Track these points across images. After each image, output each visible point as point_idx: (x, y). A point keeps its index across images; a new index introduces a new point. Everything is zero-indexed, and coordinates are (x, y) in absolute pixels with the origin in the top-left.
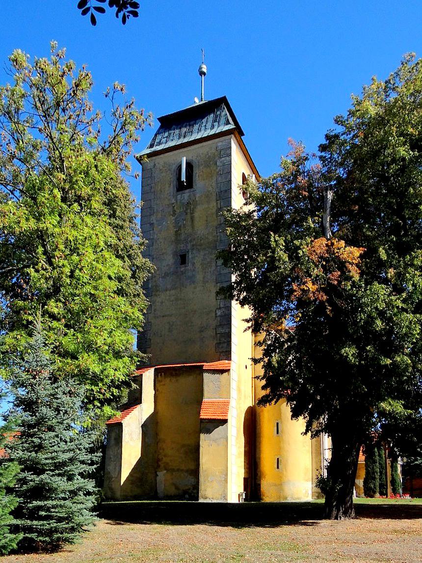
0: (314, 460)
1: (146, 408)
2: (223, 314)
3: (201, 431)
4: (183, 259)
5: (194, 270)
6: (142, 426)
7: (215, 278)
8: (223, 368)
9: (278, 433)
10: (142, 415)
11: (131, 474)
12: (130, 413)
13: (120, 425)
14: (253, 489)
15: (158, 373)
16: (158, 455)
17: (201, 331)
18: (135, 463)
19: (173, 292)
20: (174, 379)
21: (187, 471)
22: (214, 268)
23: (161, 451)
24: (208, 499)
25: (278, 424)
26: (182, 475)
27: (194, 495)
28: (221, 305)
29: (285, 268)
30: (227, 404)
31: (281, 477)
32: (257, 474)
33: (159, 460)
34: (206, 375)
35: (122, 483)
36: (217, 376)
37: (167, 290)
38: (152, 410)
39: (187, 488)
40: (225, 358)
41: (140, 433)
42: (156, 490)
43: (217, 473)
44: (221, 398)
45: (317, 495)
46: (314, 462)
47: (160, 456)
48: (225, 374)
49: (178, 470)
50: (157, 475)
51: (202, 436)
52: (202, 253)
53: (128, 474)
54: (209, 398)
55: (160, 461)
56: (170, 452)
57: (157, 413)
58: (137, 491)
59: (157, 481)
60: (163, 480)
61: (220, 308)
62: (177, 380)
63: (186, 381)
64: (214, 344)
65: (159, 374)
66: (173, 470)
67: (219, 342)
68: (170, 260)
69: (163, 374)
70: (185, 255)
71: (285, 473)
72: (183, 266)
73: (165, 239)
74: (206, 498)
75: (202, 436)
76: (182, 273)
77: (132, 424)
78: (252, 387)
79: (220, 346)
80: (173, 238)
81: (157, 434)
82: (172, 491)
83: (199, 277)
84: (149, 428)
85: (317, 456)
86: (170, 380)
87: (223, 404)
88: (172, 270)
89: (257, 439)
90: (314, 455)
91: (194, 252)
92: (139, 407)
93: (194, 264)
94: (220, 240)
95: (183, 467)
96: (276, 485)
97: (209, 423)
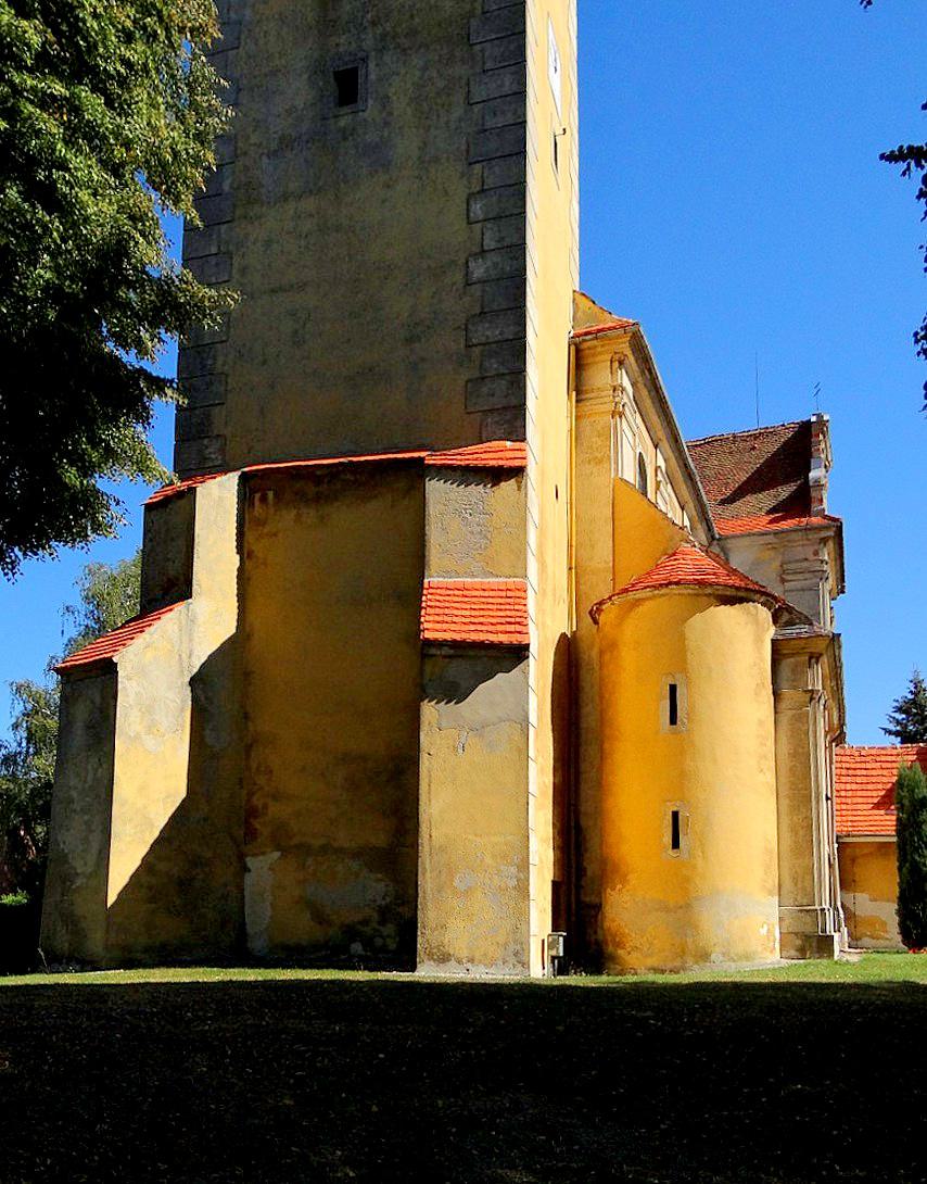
0: (785, 821)
1: (209, 617)
2: (493, 273)
3: (422, 693)
4: (346, 86)
5: (386, 124)
6: (194, 682)
7: (464, 147)
8: (501, 463)
9: (673, 720)
10: (191, 640)
11: (147, 865)
12: (147, 629)
13: (108, 669)
14: (573, 919)
15: (253, 492)
16: (251, 794)
17: (410, 340)
18: (161, 821)
19: (309, 204)
20: (310, 515)
21: (357, 854)
22: (458, 112)
23: (262, 780)
24: (453, 962)
25: (673, 689)
26: (340, 867)
27: (384, 945)
28: (486, 242)
29: (159, 934)
30: (518, 594)
31: (687, 880)
32: (585, 870)
33: (252, 813)
34: (435, 488)
35: (112, 899)
36: (476, 491)
37: (286, 200)
38: (228, 628)
39: (358, 917)
40: (500, 432)
41: (182, 710)
42: (244, 924)
43: (489, 860)
44: (492, 574)
45: (798, 942)
46: (784, 828)
47: (255, 799)
48: (508, 486)
49: (325, 849)
50: (246, 869)
51: (430, 711)
52: (417, 61)
53: (138, 863)
54: (447, 573)
55: (256, 817)
56: (298, 785)
57: (249, 637)
58: (171, 929)
59: (246, 893)
60: (268, 886)
61: (483, 252)
62: (322, 518)
63: (355, 523)
64: (461, 383)
65: (258, 496)
66: (304, 850)
67: (477, 374)
68: (298, 92)
69: (271, 495)
70: (354, 72)
71: (700, 862)
72: (346, 109)
73: (282, 19)
74: (444, 959)
75: (430, 711)
76: (346, 134)
77: (158, 672)
78: (570, 569)
79: (485, 390)
80: (311, 17)
81: (246, 716)
82: (303, 928)
83: (406, 146)
84: (218, 691)
85: (794, 809)
86: (299, 516)
87: (504, 594)
88: (305, 126)
89: (582, 750)
90: (785, 802)
91: (387, 58)
92: (179, 608)
93: (385, 101)
94: (484, 13)
95: (343, 839)
96: (667, 909)
97: (455, 662)
